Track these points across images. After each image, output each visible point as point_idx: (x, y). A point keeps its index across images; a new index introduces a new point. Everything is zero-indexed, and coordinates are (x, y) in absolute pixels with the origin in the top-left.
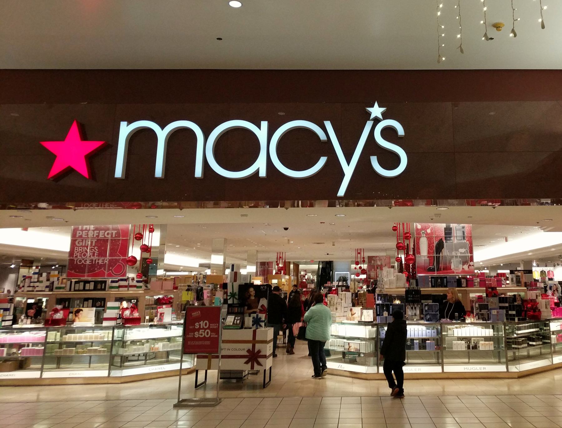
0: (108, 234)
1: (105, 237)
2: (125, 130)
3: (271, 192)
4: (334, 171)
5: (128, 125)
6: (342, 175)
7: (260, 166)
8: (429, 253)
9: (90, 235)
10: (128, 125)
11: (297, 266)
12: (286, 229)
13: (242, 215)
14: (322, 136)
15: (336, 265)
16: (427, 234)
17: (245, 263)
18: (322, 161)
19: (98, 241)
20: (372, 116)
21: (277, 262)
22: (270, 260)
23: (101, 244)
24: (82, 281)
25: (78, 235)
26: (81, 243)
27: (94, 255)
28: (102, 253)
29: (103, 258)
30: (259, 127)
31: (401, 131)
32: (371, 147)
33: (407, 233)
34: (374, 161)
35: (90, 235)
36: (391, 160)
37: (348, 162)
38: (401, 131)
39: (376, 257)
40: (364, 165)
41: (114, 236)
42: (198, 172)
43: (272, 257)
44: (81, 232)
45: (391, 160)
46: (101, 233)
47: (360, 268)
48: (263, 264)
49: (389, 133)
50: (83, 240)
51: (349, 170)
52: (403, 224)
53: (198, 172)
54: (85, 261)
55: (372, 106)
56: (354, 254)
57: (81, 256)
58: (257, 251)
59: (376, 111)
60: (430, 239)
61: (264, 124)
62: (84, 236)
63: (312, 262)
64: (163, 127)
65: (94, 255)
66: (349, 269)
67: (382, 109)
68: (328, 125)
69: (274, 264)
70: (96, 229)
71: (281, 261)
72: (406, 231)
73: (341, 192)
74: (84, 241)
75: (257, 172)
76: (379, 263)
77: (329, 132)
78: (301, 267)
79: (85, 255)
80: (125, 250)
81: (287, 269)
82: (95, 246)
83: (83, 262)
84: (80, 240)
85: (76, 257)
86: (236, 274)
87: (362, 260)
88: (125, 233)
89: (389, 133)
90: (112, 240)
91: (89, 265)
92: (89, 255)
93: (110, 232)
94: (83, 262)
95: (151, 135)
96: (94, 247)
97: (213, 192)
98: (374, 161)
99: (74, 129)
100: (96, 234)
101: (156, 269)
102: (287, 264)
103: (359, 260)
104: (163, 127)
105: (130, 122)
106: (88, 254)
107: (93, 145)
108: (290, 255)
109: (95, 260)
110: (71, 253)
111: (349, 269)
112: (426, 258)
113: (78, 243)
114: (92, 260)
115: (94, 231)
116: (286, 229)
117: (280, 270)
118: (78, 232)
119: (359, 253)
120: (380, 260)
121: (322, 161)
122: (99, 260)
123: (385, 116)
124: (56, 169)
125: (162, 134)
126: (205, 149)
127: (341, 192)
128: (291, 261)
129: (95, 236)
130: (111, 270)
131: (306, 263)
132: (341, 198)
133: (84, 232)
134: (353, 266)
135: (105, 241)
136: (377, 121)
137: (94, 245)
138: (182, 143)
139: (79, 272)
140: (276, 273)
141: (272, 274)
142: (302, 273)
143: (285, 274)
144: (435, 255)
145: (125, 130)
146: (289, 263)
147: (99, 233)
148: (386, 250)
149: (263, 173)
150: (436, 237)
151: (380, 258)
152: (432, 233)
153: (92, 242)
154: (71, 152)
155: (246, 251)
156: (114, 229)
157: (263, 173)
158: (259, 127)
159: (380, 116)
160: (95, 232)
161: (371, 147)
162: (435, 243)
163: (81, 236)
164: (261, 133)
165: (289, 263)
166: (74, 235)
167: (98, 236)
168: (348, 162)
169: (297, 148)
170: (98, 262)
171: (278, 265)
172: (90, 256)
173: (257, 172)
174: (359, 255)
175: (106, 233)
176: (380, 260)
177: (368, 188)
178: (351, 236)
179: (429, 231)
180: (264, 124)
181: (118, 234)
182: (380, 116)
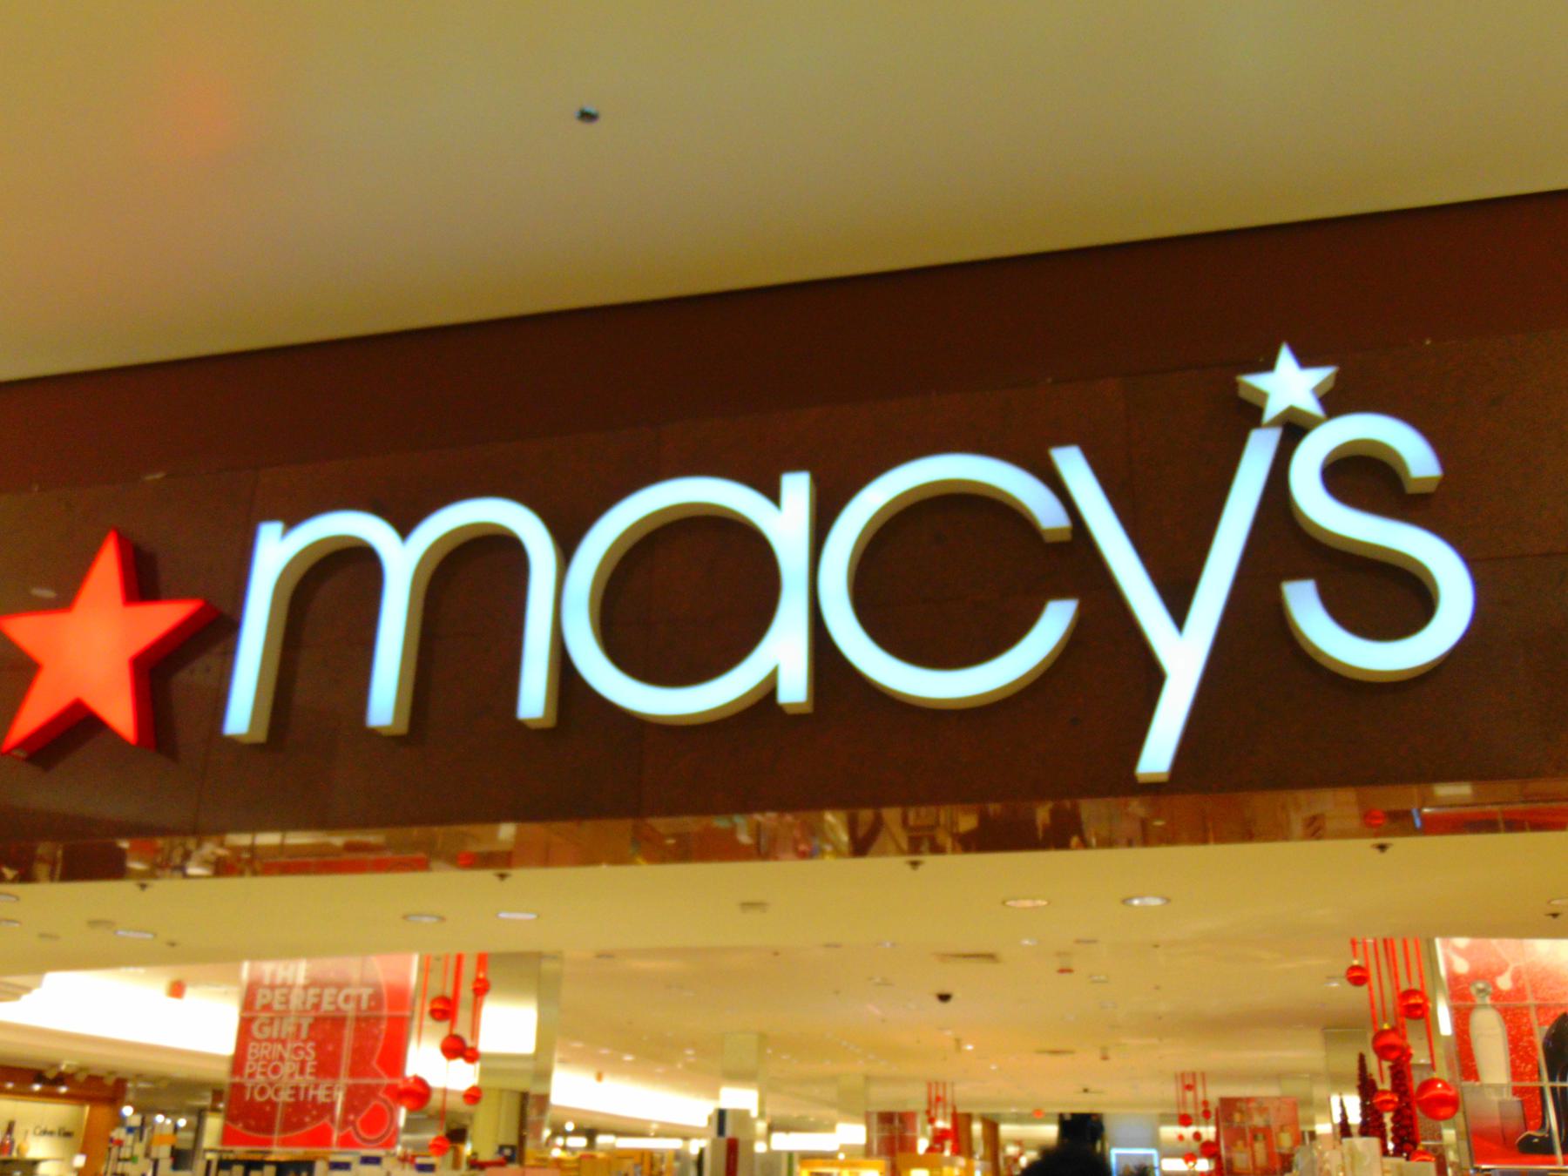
0: (347, 999)
1: (338, 1009)
2: (276, 551)
3: (836, 770)
4: (1110, 663)
5: (285, 533)
6: (1151, 677)
7: (780, 661)
8: (1516, 1074)
9: (295, 1002)
10: (285, 533)
11: (992, 1126)
12: (944, 998)
13: (747, 906)
14: (1045, 511)
15: (1112, 1128)
16: (1497, 995)
17: (833, 1113)
18: (1054, 623)
19: (318, 1022)
20: (1273, 409)
21: (928, 1112)
22: (910, 1107)
23: (326, 1028)
24: (237, 1162)
25: (260, 1002)
26: (267, 1030)
27: (302, 1071)
28: (326, 1067)
29: (327, 1083)
30: (773, 494)
31: (1417, 456)
32: (1282, 539)
33: (1411, 993)
34: (1305, 608)
35: (295, 1002)
36: (1390, 597)
37: (1178, 605)
38: (1417, 456)
39: (1248, 1100)
40: (1254, 624)
41: (364, 1005)
42: (534, 698)
43: (913, 1098)
44: (267, 992)
45: (1390, 597)
46: (328, 994)
47: (1197, 1136)
48: (887, 1118)
49: (1359, 476)
50: (272, 1019)
51: (1182, 652)
52: (1416, 943)
53: (534, 698)
54: (277, 1092)
55: (1268, 365)
56: (1171, 1092)
57: (264, 1074)
58: (764, 1039)
59: (1289, 384)
60: (1513, 1018)
61: (797, 487)
62: (277, 1006)
63: (1037, 1117)
64: (404, 528)
65: (302, 1071)
66: (1155, 1142)
67: (1319, 375)
68: (1072, 464)
69: (921, 1120)
70: (313, 983)
71: (940, 1111)
72: (1404, 986)
73: (1158, 753)
74: (276, 1023)
75: (769, 688)
76: (1258, 1121)
77: (1073, 493)
78: (1006, 1130)
79: (276, 1070)
80: (394, 1057)
81: (963, 1137)
82: (309, 1039)
83: (270, 1093)
84: (264, 1016)
85: (252, 1075)
86: (733, 1147)
87: (1201, 1109)
88: (399, 997)
89: (1359, 476)
90: (358, 1019)
91: (287, 1105)
92: (288, 1075)
93: (352, 992)
94: (270, 1093)
95: (359, 564)
96: (305, 1041)
97: (603, 787)
98: (1305, 608)
99: (107, 569)
100: (311, 1000)
101: (751, 1143)
102: (961, 1122)
103: (1190, 1111)
104: (404, 528)
105: (292, 520)
106: (286, 1069)
107: (162, 618)
108: (969, 1093)
109: (307, 1090)
110: (238, 1062)
111: (1155, 1142)
112: (1508, 1096)
113: (260, 1029)
114: (297, 1089)
115: (306, 988)
116: (944, 998)
117: (939, 1138)
118: (261, 992)
119: (1189, 1087)
120: (1263, 1110)
121: (1054, 623)
122: (316, 1087)
123: (1335, 402)
124: (36, 712)
125: (402, 559)
126: (560, 604)
127: (1158, 753)
128: (975, 1111)
129: (308, 1006)
130: (353, 1123)
131: (1019, 1119)
132: (1153, 788)
133: (278, 992)
134: (1170, 1132)
135: (338, 1021)
136: (1294, 429)
137: (304, 1034)
138: (477, 587)
139: (258, 1129)
140: (930, 1150)
141: (913, 1148)
142: (1011, 1150)
143: (957, 1151)
144: (1546, 1084)
145: (276, 551)
146: (969, 1118)
147: (320, 996)
148: (1278, 1077)
149: (794, 690)
150: (1539, 1008)
151: (1262, 1106)
152: (1518, 992)
153: (299, 1027)
154: (90, 649)
155: (833, 1079)
156: (364, 984)
157: (794, 690)
158: (773, 494)
159: (1311, 406)
160: (312, 991)
161: (1282, 539)
162: (1540, 1035)
163: (267, 1007)
164: (783, 518)
165: (969, 1118)
166: (248, 1003)
167: (317, 1006)
168: (1178, 605)
169: (939, 578)
170: (315, 1097)
171: (931, 1121)
172: (292, 1075)
173: (769, 688)
174: (1190, 1095)
175: (341, 998)
176: (1263, 1110)
177: (1288, 742)
178: (1160, 1027)
179: (1504, 983)
180: (797, 487)
181: (376, 998)
182: (1311, 406)
